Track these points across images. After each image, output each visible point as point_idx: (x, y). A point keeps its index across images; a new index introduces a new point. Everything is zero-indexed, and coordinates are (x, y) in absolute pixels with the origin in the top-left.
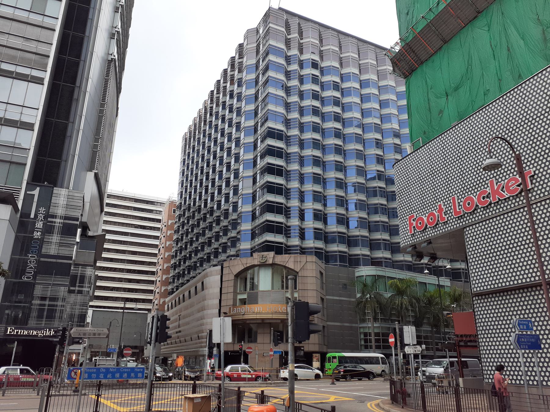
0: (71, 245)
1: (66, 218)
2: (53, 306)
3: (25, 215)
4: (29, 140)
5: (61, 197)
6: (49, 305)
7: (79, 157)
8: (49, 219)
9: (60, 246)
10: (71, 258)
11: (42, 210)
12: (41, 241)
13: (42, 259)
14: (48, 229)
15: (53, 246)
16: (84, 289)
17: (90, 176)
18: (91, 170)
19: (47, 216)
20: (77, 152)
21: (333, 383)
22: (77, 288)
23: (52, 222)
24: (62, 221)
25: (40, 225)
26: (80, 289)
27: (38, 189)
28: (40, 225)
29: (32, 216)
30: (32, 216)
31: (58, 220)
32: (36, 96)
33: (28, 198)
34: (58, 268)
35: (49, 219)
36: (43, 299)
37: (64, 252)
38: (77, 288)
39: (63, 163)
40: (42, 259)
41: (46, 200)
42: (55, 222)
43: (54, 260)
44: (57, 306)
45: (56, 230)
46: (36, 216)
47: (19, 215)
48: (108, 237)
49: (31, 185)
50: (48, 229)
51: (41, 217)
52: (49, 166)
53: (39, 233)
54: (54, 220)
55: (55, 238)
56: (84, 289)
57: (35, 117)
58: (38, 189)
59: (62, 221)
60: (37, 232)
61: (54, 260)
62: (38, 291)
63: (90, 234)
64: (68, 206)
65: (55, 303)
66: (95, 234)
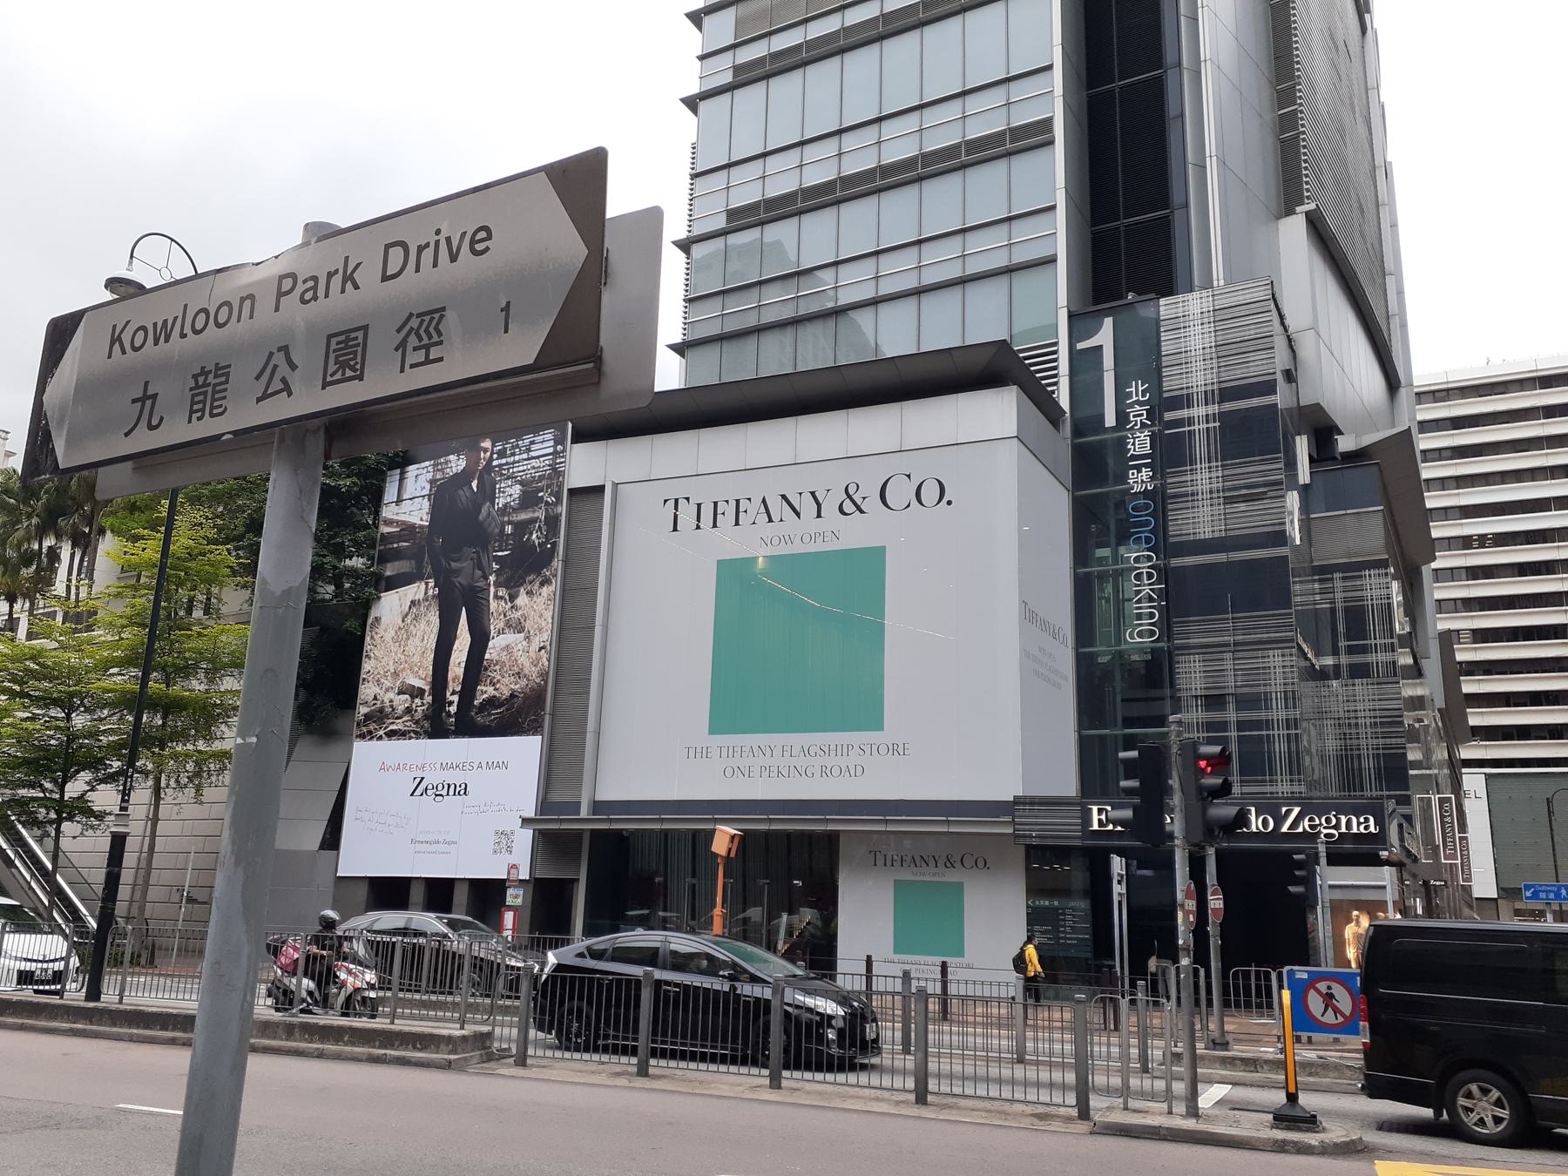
0: (1276, 488)
1: (1226, 394)
2: (1258, 724)
3: (1086, 423)
4: (1050, 176)
5: (1189, 324)
6: (1241, 725)
7: (1222, 163)
8: (1168, 416)
9: (1229, 501)
10: (1280, 538)
11: (1137, 390)
12: (1159, 500)
13: (1176, 562)
14: (1171, 452)
15: (1204, 510)
16: (1371, 658)
17: (1294, 228)
18: (1289, 212)
19: (1160, 404)
20: (1211, 146)
21: (643, 1071)
22: (1344, 660)
23: (1179, 423)
24: (1214, 409)
26: (1358, 659)
27: (1108, 322)
28: (1140, 443)
29: (1110, 420)
30: (1110, 420)
31: (1199, 411)
33: (1085, 363)
34: (1243, 584)
35: (1168, 416)
36: (1214, 701)
37: (1249, 518)
38: (1344, 660)
39: (1178, 216)
40: (1176, 562)
41: (1143, 356)
42: (1190, 421)
43: (1221, 557)
44: (1268, 724)
45: (1200, 448)
46: (1122, 417)
47: (1067, 429)
48: (1425, 442)
49: (1081, 321)
50: (1171, 452)
51: (1137, 415)
52: (1130, 235)
53: (1145, 474)
54: (1184, 413)
55: (1204, 477)
56: (1371, 658)
57: (1051, 101)
58: (1108, 322)
59: (1214, 409)
60: (1138, 468)
61: (1221, 557)
62: (1192, 675)
63: (1345, 444)
64: (1224, 351)
65: (1262, 715)
66: (1368, 439)
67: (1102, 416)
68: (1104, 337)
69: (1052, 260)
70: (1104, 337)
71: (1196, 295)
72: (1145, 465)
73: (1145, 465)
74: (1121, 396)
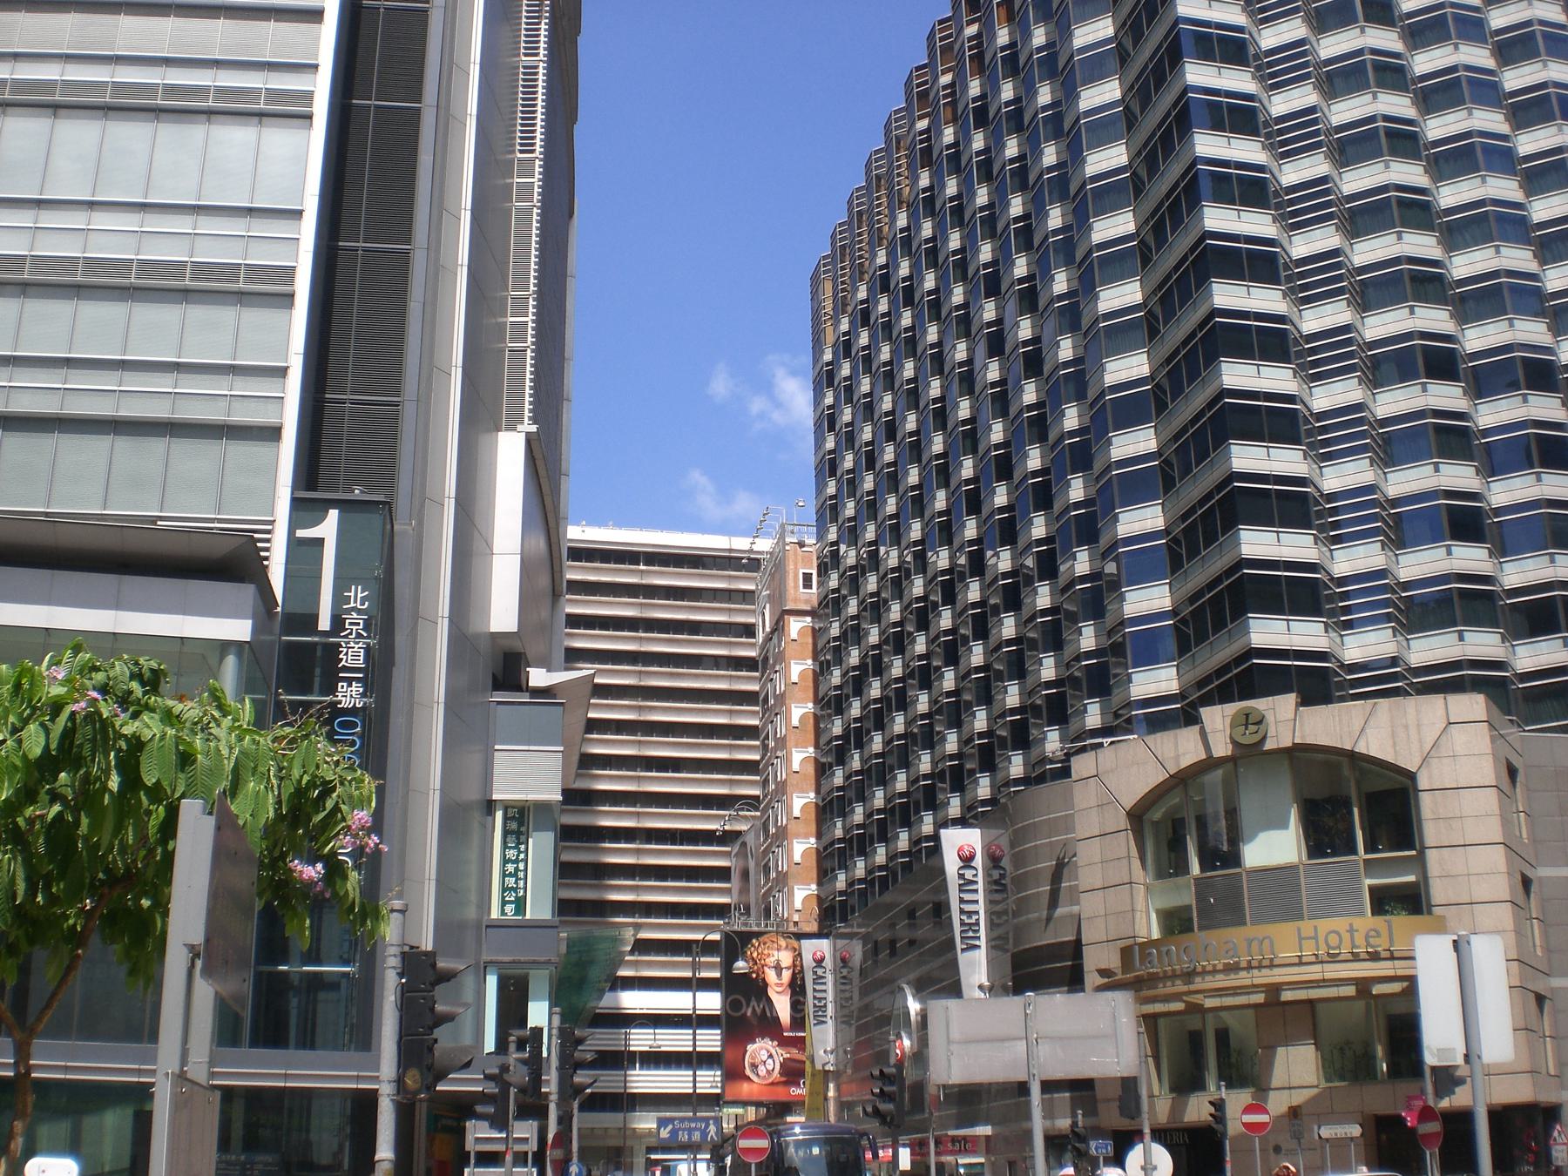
11: (357, 596)
25: (353, 654)
29: (324, 624)
30: (324, 624)
32: (297, 162)
46: (338, 623)
49: (305, 508)
51: (355, 622)
53: (356, 688)
58: (333, 514)
67: (315, 618)
68: (328, 528)
69: (282, 372)
70: (328, 528)
71: (314, 1137)
72: (358, 680)
73: (358, 680)
74: (339, 598)
